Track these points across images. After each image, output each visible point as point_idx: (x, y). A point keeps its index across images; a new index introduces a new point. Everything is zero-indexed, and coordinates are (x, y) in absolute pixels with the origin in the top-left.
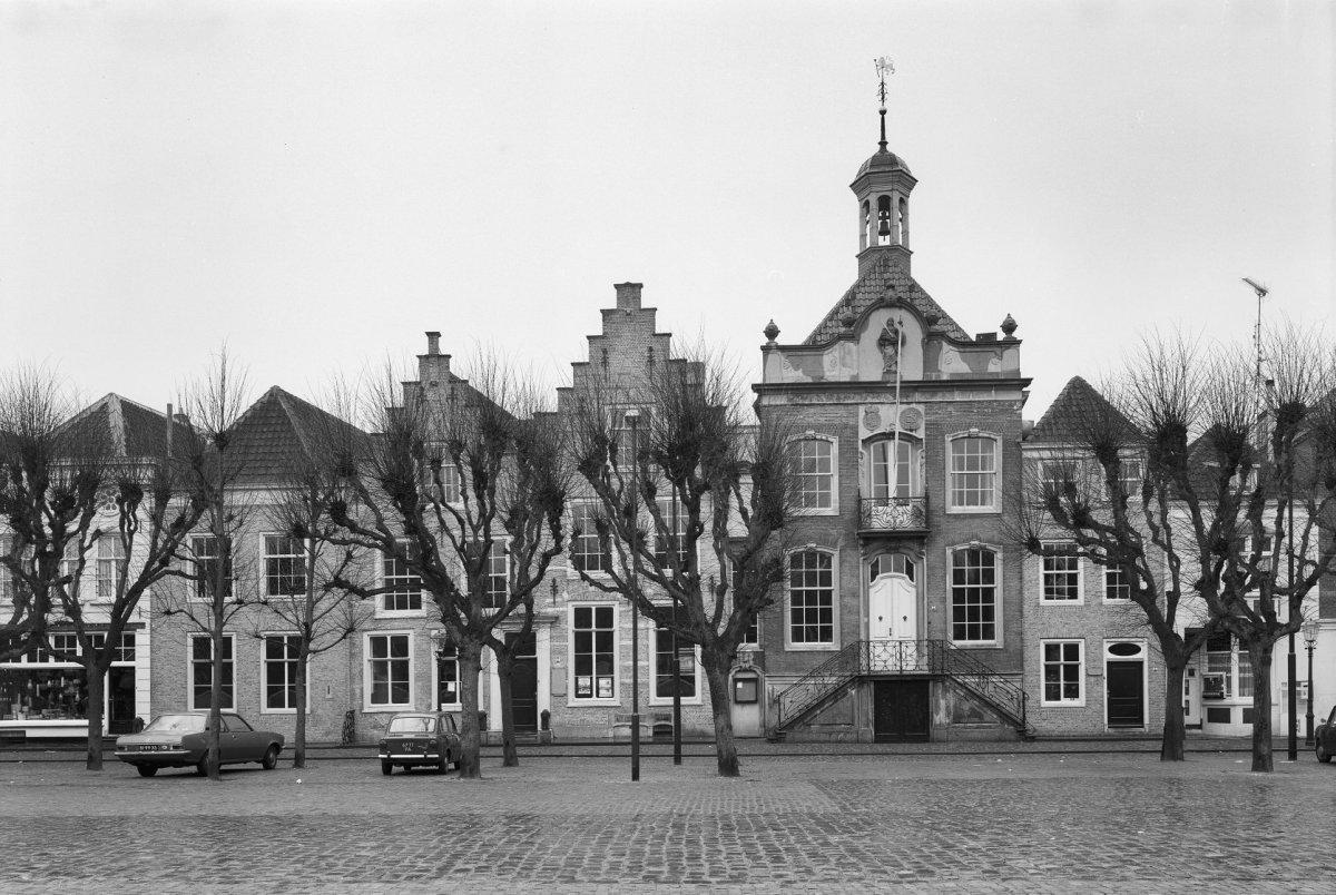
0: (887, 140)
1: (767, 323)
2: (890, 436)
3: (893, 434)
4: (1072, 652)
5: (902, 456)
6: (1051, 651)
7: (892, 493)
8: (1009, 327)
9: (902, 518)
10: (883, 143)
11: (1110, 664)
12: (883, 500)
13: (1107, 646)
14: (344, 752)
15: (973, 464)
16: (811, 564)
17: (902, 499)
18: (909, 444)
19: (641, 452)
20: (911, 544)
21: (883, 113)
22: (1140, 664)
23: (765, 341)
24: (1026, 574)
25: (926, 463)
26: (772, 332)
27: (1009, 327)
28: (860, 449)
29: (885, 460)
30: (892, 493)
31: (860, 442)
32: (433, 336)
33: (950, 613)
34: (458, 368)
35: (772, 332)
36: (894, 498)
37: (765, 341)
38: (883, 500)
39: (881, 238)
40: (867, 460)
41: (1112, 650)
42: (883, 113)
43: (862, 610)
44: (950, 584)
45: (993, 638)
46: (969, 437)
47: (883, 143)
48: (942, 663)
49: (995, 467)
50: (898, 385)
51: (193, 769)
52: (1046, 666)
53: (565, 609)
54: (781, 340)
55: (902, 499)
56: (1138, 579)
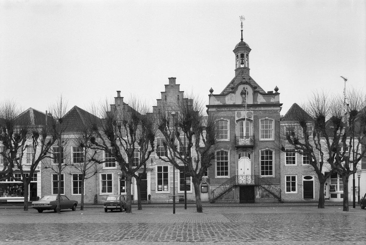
0: (243, 38)
1: (210, 88)
2: (244, 119)
3: (245, 119)
4: (294, 178)
5: (247, 125)
6: (288, 178)
7: (244, 135)
8: (276, 89)
9: (247, 142)
10: (242, 39)
11: (304, 182)
12: (242, 137)
13: (303, 177)
14: (94, 206)
15: (266, 127)
16: (222, 154)
17: (247, 137)
18: (249, 122)
19: (176, 124)
20: (250, 149)
21: (242, 31)
22: (312, 182)
23: (210, 93)
24: (281, 157)
25: (254, 127)
26: (211, 91)
27: (276, 89)
28: (236, 123)
29: (243, 126)
30: (244, 135)
31: (236, 121)
32: (119, 92)
33: (260, 168)
34: (125, 101)
35: (211, 91)
36: (245, 136)
37: (210, 93)
38: (242, 137)
39: (241, 65)
40: (238, 126)
41: (305, 178)
42: (242, 31)
43: (236, 167)
44: (260, 160)
45: (272, 175)
46: (265, 120)
47: (242, 39)
48: (258, 182)
49: (273, 128)
50: (246, 105)
51: (53, 210)
52: (287, 182)
53: (155, 167)
54: (214, 93)
55: (247, 137)
56: (312, 159)
